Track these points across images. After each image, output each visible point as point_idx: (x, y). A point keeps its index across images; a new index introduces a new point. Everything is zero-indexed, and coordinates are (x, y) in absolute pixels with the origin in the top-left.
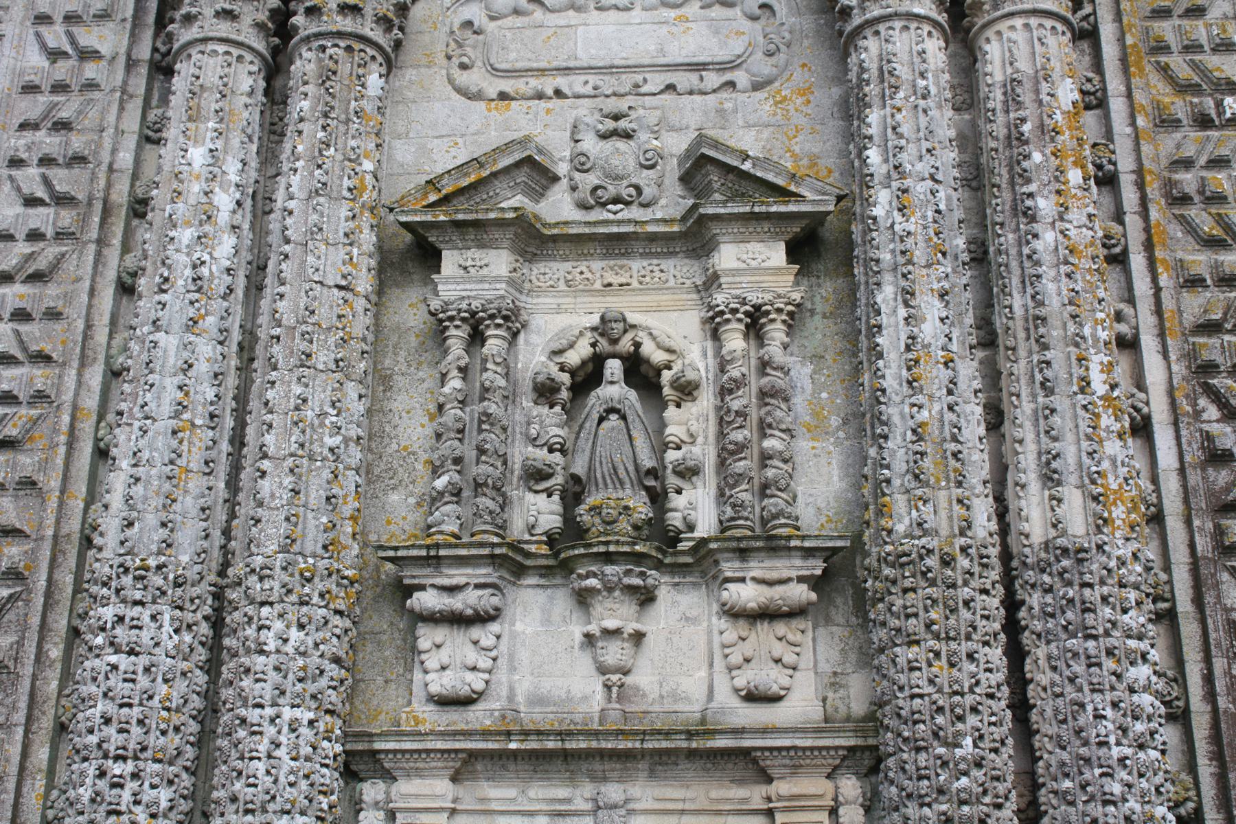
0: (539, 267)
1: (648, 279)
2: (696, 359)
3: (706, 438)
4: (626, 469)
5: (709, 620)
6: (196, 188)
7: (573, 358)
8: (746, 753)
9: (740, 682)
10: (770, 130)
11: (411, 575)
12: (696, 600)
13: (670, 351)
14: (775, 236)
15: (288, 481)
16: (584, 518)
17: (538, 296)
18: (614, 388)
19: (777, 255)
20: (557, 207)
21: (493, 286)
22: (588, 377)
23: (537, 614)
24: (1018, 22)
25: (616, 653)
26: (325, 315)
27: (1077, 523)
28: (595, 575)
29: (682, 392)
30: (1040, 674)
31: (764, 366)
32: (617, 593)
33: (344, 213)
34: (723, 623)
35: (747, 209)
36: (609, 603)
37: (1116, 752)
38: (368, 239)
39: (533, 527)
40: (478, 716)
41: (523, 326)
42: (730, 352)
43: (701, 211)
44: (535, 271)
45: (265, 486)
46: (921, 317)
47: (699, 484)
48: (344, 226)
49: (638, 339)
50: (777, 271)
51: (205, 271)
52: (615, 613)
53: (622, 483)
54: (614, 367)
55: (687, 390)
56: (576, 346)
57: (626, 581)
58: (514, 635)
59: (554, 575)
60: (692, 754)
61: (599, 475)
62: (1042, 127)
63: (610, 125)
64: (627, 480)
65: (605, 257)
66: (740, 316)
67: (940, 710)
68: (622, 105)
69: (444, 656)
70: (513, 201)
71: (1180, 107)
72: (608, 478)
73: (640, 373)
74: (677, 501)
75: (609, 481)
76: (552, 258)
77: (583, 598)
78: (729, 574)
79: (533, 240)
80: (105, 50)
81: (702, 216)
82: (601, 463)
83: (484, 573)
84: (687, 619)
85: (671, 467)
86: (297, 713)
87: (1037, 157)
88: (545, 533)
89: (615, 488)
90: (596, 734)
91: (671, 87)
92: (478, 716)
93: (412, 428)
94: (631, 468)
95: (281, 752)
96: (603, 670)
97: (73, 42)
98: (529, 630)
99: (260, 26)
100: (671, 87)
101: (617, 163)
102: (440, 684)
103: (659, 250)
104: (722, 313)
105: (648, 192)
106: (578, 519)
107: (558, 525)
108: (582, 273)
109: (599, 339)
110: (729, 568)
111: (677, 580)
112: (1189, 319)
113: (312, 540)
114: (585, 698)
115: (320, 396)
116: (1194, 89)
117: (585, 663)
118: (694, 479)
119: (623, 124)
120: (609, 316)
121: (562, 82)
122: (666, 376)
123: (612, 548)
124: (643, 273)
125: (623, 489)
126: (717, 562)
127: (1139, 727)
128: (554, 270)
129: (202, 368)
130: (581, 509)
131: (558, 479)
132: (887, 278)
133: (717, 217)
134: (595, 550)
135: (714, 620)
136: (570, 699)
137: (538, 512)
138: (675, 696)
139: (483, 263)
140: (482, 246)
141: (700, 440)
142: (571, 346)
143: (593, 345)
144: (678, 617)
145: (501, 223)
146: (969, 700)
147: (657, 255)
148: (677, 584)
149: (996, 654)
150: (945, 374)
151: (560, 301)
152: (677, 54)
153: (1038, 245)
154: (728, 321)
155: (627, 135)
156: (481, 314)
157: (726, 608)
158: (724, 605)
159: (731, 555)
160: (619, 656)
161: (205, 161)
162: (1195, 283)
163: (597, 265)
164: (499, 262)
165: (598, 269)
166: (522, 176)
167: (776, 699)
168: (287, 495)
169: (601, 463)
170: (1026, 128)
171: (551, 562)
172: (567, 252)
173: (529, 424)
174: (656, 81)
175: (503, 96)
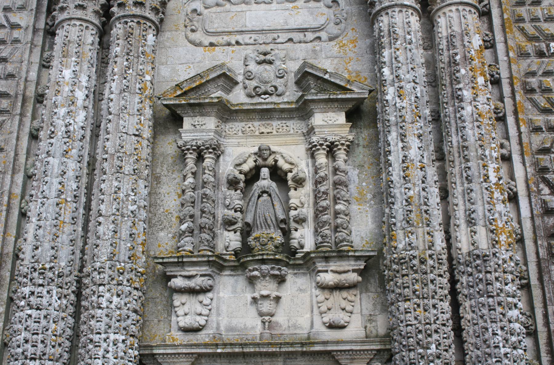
0: (229, 125)
1: (280, 130)
2: (304, 167)
3: (309, 204)
4: (271, 219)
5: (311, 290)
6: (67, 89)
7: (246, 167)
8: (329, 353)
9: (326, 319)
10: (338, 59)
11: (170, 271)
12: (305, 281)
13: (291, 164)
14: (340, 109)
15: (112, 227)
16: (252, 243)
17: (229, 139)
18: (265, 181)
19: (341, 118)
20: (238, 97)
21: (208, 134)
22: (253, 176)
23: (230, 288)
24: (453, 8)
25: (267, 306)
26: (128, 148)
27: (483, 243)
28: (257, 270)
29: (297, 183)
30: (467, 315)
31: (336, 170)
32: (267, 278)
33: (137, 100)
34: (318, 292)
35: (327, 97)
36: (263, 283)
37: (503, 351)
38: (148, 112)
39: (228, 247)
40: (203, 337)
41: (222, 153)
42: (320, 164)
43: (306, 98)
44: (228, 127)
45: (101, 229)
46: (410, 147)
47: (306, 226)
48: (137, 106)
49: (276, 158)
50: (341, 126)
51: (71, 128)
52: (267, 288)
53: (269, 226)
54: (265, 172)
55: (299, 182)
56: (247, 162)
57: (272, 272)
58: (219, 298)
59: (238, 270)
60: (303, 354)
61: (258, 223)
62: (465, 57)
63: (262, 57)
64: (272, 225)
65: (260, 119)
66: (324, 147)
67: (420, 332)
68: (268, 48)
69: (186, 309)
70: (217, 94)
71: (529, 48)
72: (262, 224)
73: (278, 175)
74: (296, 235)
75: (263, 225)
76: (236, 120)
77: (252, 281)
78: (320, 269)
79: (227, 112)
80: (23, 24)
81: (306, 100)
82: (259, 217)
83: (205, 269)
84: (301, 290)
85: (292, 218)
86: (117, 336)
87: (463, 71)
88: (233, 250)
89: (266, 229)
90: (258, 345)
91: (290, 40)
92: (203, 337)
93: (170, 201)
94: (274, 219)
95: (110, 355)
96: (261, 314)
97: (8, 20)
98: (226, 296)
99: (96, 12)
100: (290, 40)
101: (266, 75)
102: (184, 322)
103: (286, 116)
104: (316, 146)
105: (280, 89)
106: (249, 243)
107: (239, 246)
108: (249, 127)
109: (258, 158)
110: (320, 265)
111: (296, 272)
112: (535, 147)
113: (123, 255)
114: (253, 328)
115: (126, 187)
116: (536, 39)
117: (252, 311)
118: (303, 224)
119: (268, 57)
120: (263, 147)
121: (239, 38)
122: (290, 175)
123: (265, 257)
124: (278, 127)
125: (270, 229)
126: (314, 263)
127: (514, 339)
128: (236, 126)
129: (71, 174)
130: (250, 239)
131: (239, 225)
132: (393, 128)
133: (313, 101)
134: (257, 258)
135: (313, 290)
136: (246, 328)
137: (230, 240)
138: (295, 326)
139: (203, 123)
140: (202, 115)
141: (306, 206)
142: (245, 162)
143: (255, 161)
144: (296, 289)
145: (211, 104)
146: (434, 327)
147: (285, 119)
148: (296, 274)
149: (446, 305)
150: (421, 174)
151: (239, 141)
152: (293, 24)
153: (464, 112)
154: (318, 149)
155: (270, 63)
156: (202, 147)
157: (319, 285)
158: (318, 283)
159: (321, 260)
160: (269, 308)
161: (71, 76)
162: (537, 130)
163: (256, 124)
164: (210, 123)
165: (257, 125)
166: (221, 82)
167: (343, 327)
168: (111, 234)
169: (259, 217)
170: (458, 58)
171: (236, 264)
172: (243, 118)
173: (225, 199)
174: (283, 37)
175: (212, 45)
